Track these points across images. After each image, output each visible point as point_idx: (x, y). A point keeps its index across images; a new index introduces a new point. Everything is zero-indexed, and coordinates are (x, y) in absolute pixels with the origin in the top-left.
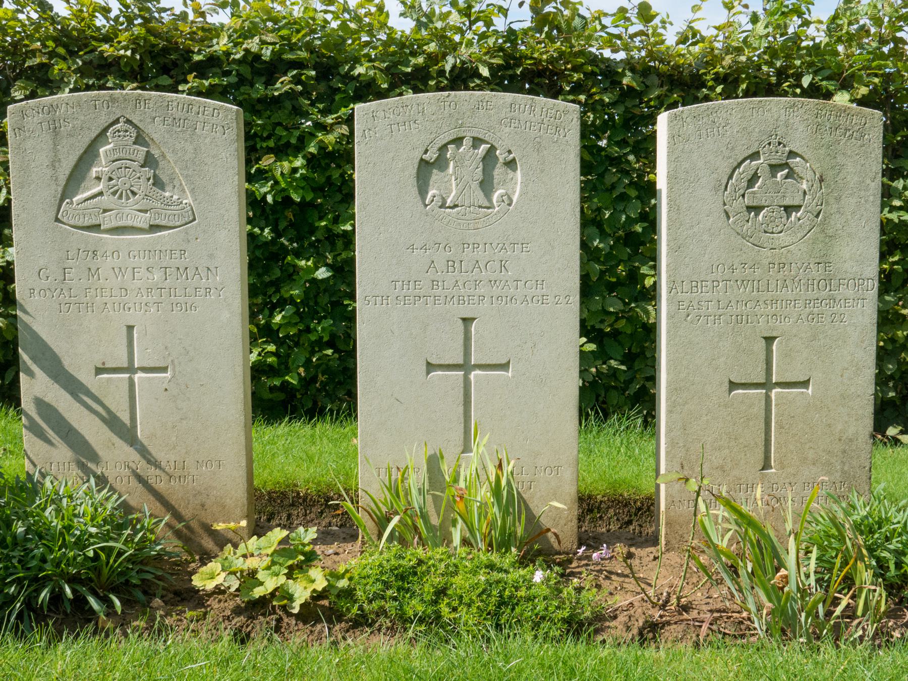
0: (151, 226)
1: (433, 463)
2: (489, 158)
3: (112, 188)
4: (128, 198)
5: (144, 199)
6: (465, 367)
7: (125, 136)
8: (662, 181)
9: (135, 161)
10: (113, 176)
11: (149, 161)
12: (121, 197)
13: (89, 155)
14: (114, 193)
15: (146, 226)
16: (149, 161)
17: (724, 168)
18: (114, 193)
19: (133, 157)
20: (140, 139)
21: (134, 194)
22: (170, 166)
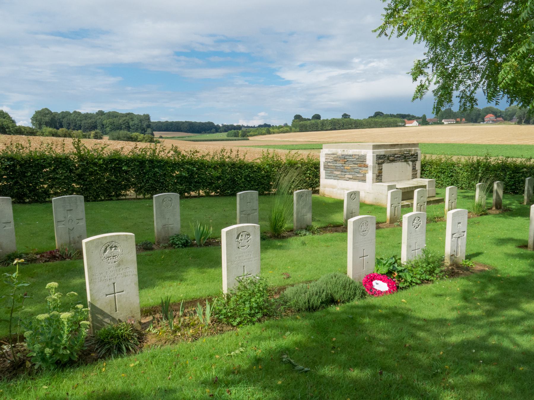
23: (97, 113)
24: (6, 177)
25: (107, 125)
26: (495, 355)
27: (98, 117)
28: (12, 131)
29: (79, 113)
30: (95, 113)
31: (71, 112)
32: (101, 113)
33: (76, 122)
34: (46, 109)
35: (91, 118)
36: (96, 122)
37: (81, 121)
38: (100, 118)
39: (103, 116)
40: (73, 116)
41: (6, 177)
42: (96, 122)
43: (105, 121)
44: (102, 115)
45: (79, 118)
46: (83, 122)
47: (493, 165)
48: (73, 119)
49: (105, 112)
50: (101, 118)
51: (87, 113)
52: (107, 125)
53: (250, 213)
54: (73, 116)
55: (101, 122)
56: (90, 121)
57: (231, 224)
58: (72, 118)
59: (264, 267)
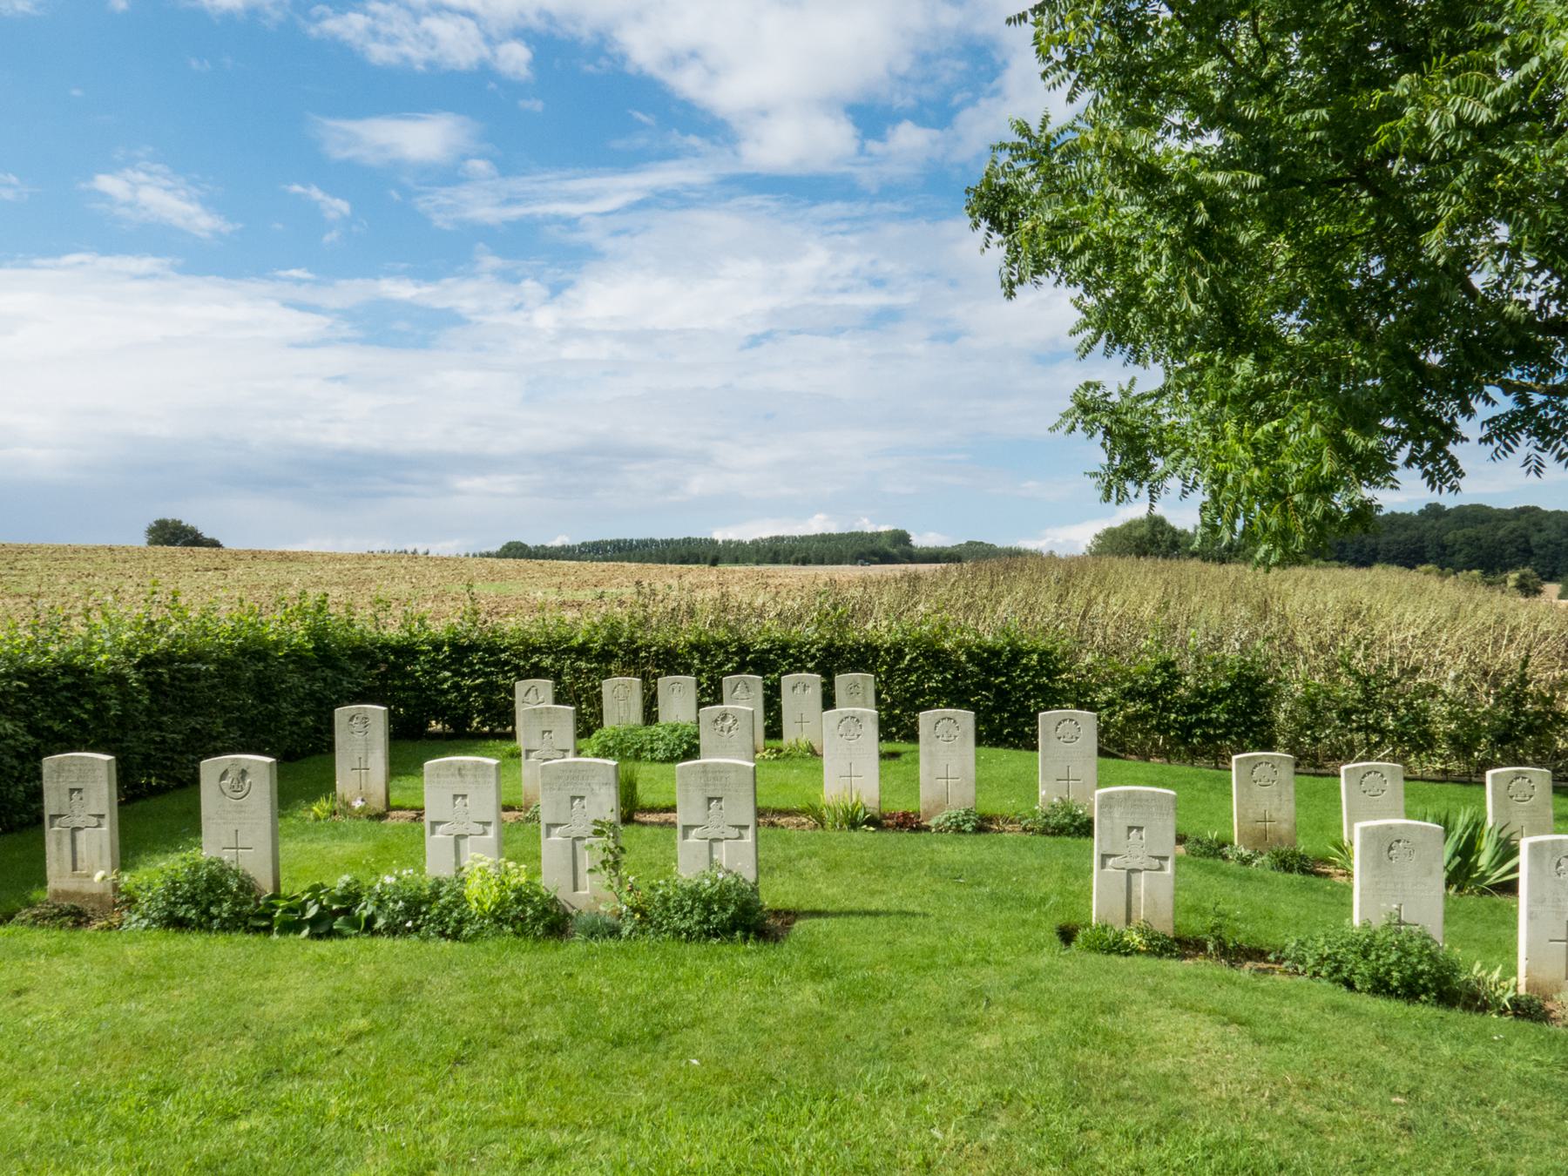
23: (1421, 512)
27: (1428, 524)
36: (1421, 539)
38: (1433, 527)
39: (1442, 520)
43: (1451, 536)
44: (1437, 518)
52: (1457, 547)
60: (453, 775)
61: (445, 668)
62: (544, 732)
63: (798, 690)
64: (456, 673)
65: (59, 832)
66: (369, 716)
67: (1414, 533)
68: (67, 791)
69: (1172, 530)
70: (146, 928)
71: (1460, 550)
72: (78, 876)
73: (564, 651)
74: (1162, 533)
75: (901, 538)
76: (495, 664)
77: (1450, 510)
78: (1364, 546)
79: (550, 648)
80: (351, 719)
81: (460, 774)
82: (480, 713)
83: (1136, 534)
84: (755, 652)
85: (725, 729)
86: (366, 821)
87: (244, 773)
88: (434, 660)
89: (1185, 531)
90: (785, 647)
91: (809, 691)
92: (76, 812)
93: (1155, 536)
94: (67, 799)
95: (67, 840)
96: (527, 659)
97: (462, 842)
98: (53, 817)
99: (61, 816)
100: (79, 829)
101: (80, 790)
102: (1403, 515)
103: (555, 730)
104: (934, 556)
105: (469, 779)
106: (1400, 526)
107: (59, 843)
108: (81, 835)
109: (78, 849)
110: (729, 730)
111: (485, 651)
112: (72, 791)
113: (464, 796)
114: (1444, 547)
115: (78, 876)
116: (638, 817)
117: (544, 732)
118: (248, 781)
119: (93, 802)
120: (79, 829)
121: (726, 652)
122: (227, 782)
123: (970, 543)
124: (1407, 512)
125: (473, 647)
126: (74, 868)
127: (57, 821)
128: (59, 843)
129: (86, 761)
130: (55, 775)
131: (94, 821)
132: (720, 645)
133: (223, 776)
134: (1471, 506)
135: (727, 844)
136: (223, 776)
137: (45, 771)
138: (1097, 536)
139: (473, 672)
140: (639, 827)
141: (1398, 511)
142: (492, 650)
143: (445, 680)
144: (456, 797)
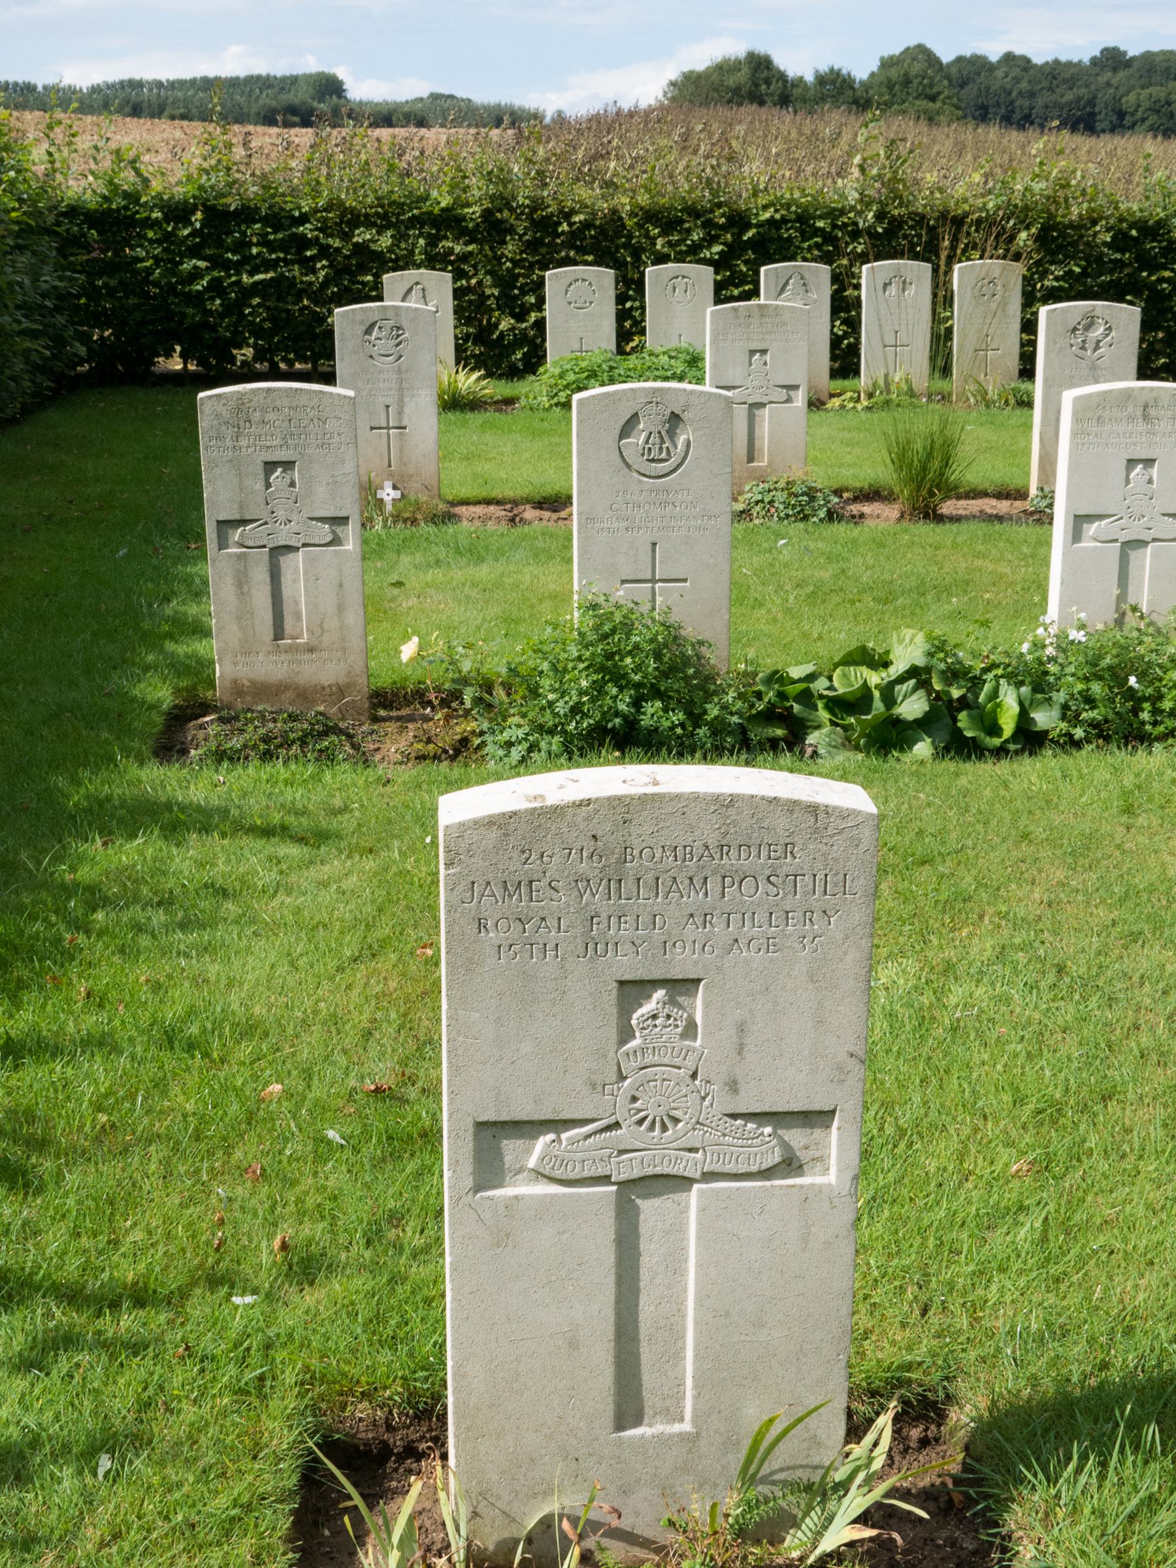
0: (704, 1174)
1: (886, 376)
2: (904, 282)
3: (635, 1114)
4: (664, 1128)
5: (694, 1129)
6: (896, 346)
7: (665, 1027)
8: (955, 287)
9: (679, 1068)
10: (637, 1094)
11: (804, 285)
12: (652, 1127)
13: (787, 283)
14: (640, 1122)
15: (698, 1175)
16: (804, 285)
17: (974, 282)
18: (640, 1122)
19: (678, 1061)
20: (802, 278)
21: (676, 1121)
22: (811, 286)
23: (1094, 61)
24: (308, 253)
25: (1139, 115)
26: (428, 805)
27: (1102, 79)
28: (432, 697)
29: (1024, 63)
30: (1086, 59)
31: (994, 58)
32: (1112, 59)
33: (1012, 102)
34: (922, 49)
35: (1072, 82)
36: (1092, 102)
37: (1032, 95)
38: (1108, 84)
39: (1122, 74)
40: (999, 73)
41: (308, 253)
42: (1092, 102)
43: (1132, 97)
44: (1115, 70)
45: (1024, 85)
46: (1040, 101)
47: (862, 83)
48: (1003, 89)
49: (1130, 54)
50: (1114, 81)
51: (1057, 62)
52: (1139, 115)
53: (764, 400)
54: (999, 73)
55: (1117, 100)
56: (1069, 97)
57: (480, 1162)
58: (998, 84)
59: (444, 453)
60: (1131, 418)
61: (195, 252)
62: (752, 352)
63: (893, 290)
64: (217, 262)
65: (240, 557)
66: (404, 323)
67: (1083, 91)
68: (260, 468)
69: (782, 76)
70: (523, 760)
71: (1143, 120)
72: (289, 650)
73: (415, 221)
74: (768, 82)
75: (330, 87)
76: (282, 246)
77: (1133, 59)
78: (1013, 112)
79: (384, 216)
80: (368, 331)
81: (1145, 417)
82: (258, 332)
83: (731, 82)
84: (759, 225)
85: (1090, 346)
86: (431, 529)
87: (675, 419)
88: (168, 237)
89: (801, 79)
90: (804, 219)
91: (911, 291)
92: (281, 514)
93: (757, 85)
94: (260, 485)
95: (260, 575)
96: (346, 237)
97: (1133, 555)
98: (225, 525)
99: (244, 522)
100: (289, 549)
101: (288, 465)
102: (1069, 64)
103: (774, 347)
104: (386, 117)
105: (1163, 426)
106: (1065, 81)
107: (242, 582)
108: (295, 566)
109: (286, 592)
110: (1097, 348)
111: (265, 220)
112: (270, 466)
113: (1149, 462)
114: (1121, 115)
115: (289, 650)
116: (948, 507)
117: (752, 352)
118: (681, 440)
119: (321, 490)
120: (289, 549)
121: (708, 224)
122: (638, 439)
123: (435, 97)
124: (1075, 60)
125: (247, 214)
126: (279, 634)
127: (236, 535)
128: (242, 582)
129: (303, 400)
130: (229, 432)
131: (324, 532)
132: (694, 212)
133: (628, 428)
134: (1163, 53)
135: (310, 561)
136: (628, 428)
137: (204, 422)
138: (673, 84)
139: (247, 259)
140: (955, 527)
141: (1155, 48)
142: (278, 219)
143: (196, 274)
144: (1131, 463)
